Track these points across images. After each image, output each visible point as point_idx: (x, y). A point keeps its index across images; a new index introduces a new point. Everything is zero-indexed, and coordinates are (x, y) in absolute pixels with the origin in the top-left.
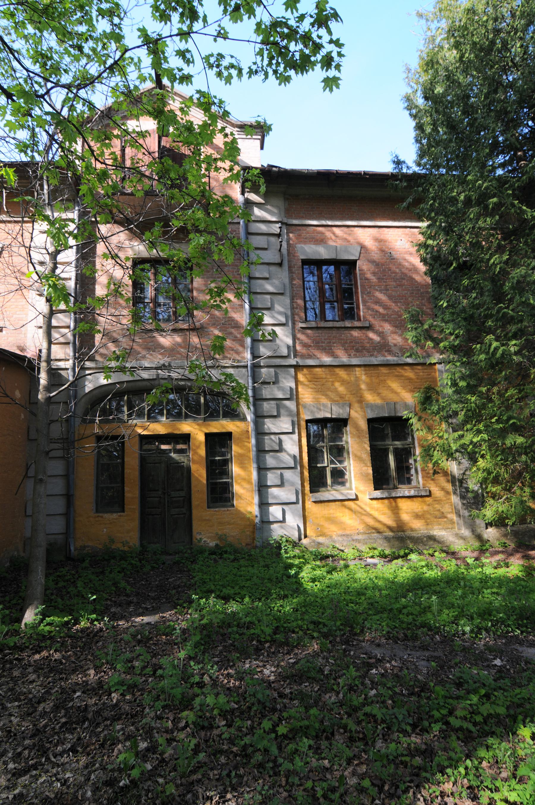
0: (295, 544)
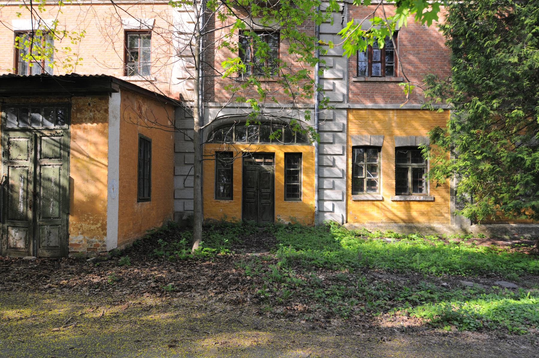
0: (339, 226)
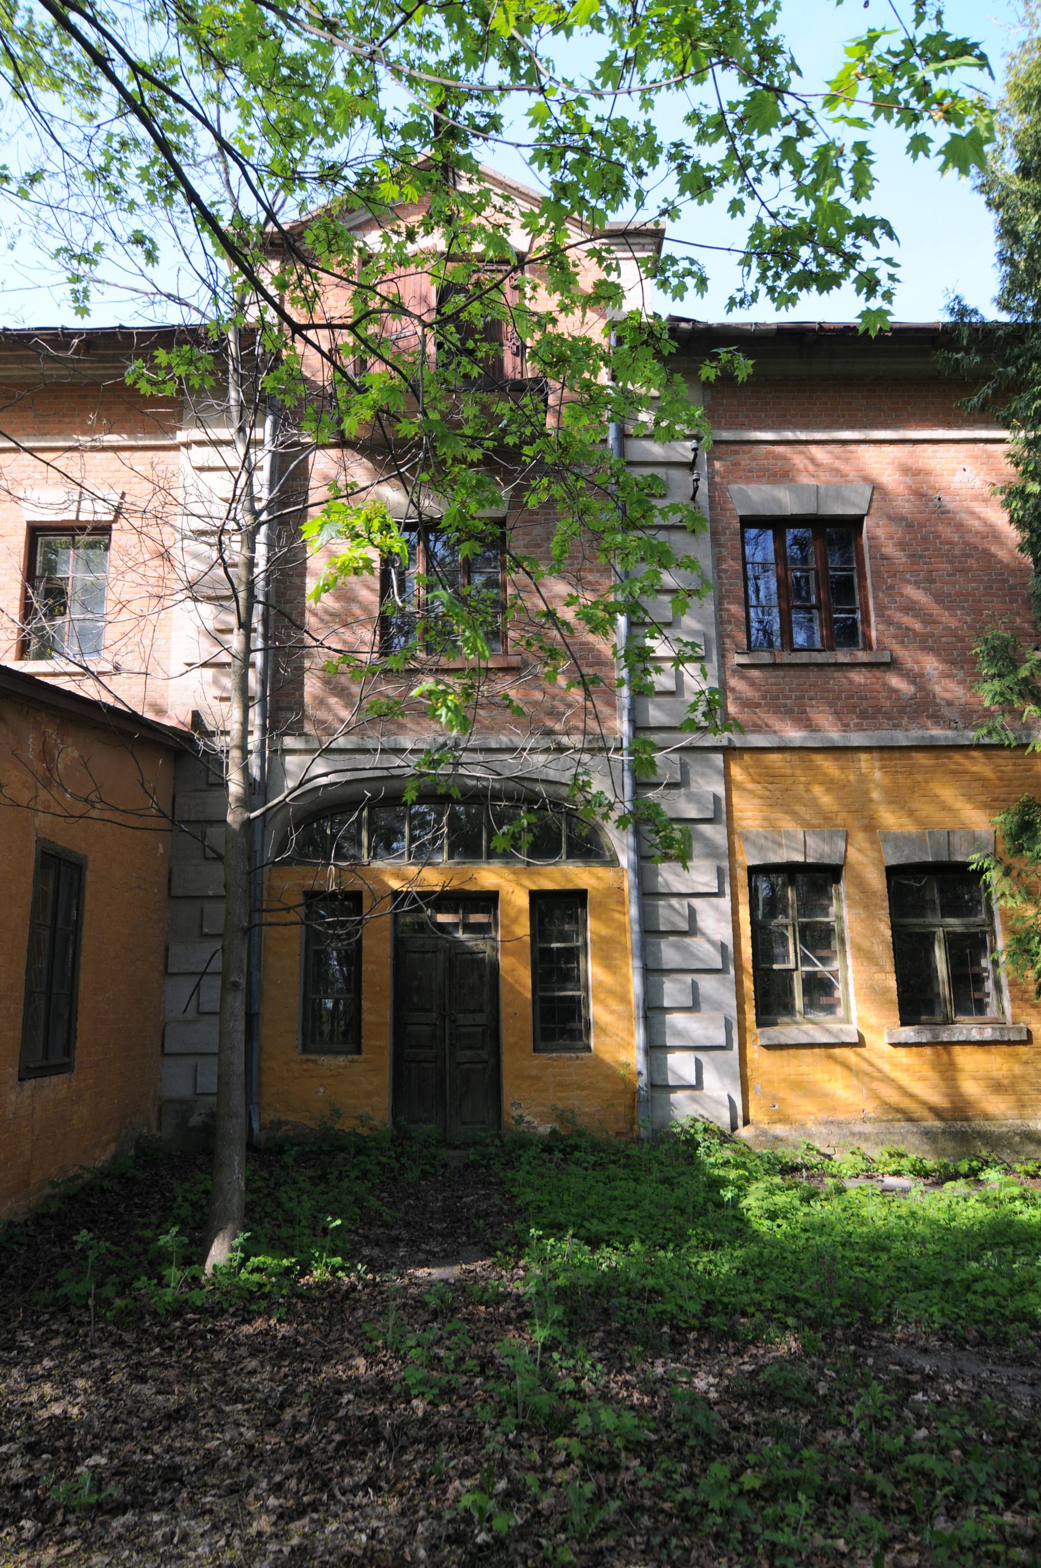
0: (725, 1138)
